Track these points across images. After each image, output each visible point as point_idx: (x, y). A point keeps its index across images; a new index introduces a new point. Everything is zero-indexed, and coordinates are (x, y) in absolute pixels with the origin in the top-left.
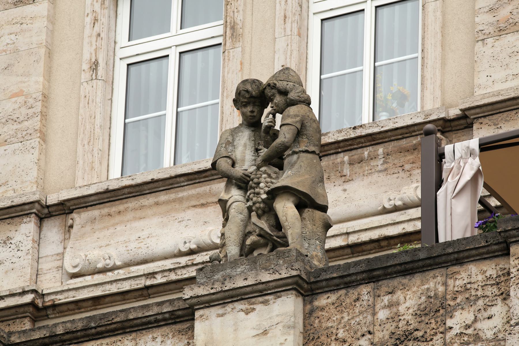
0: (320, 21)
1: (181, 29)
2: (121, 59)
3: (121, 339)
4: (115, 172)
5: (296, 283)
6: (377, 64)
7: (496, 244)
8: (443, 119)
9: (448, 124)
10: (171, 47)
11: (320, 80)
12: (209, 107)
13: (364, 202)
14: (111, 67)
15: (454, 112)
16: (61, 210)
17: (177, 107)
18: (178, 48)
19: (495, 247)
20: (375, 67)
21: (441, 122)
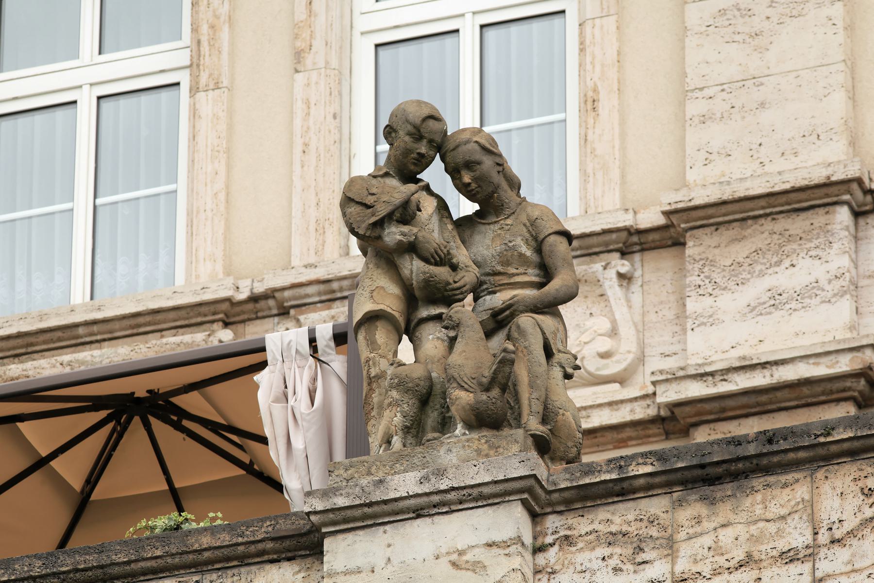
0: (373, 48)
1: (100, 53)
2: (362, 34)
3: (609, 516)
4: (79, 294)
5: (529, 490)
6: (98, 201)
7: (273, 539)
8: (228, 300)
9: (635, 239)
10: (81, 87)
11: (95, 207)
12: (162, 197)
13: (623, 348)
14: (346, 48)
15: (650, 218)
16: (326, 293)
17: (95, 197)
18: (477, 16)
19: (270, 545)
20: (95, 207)
21: (624, 235)
